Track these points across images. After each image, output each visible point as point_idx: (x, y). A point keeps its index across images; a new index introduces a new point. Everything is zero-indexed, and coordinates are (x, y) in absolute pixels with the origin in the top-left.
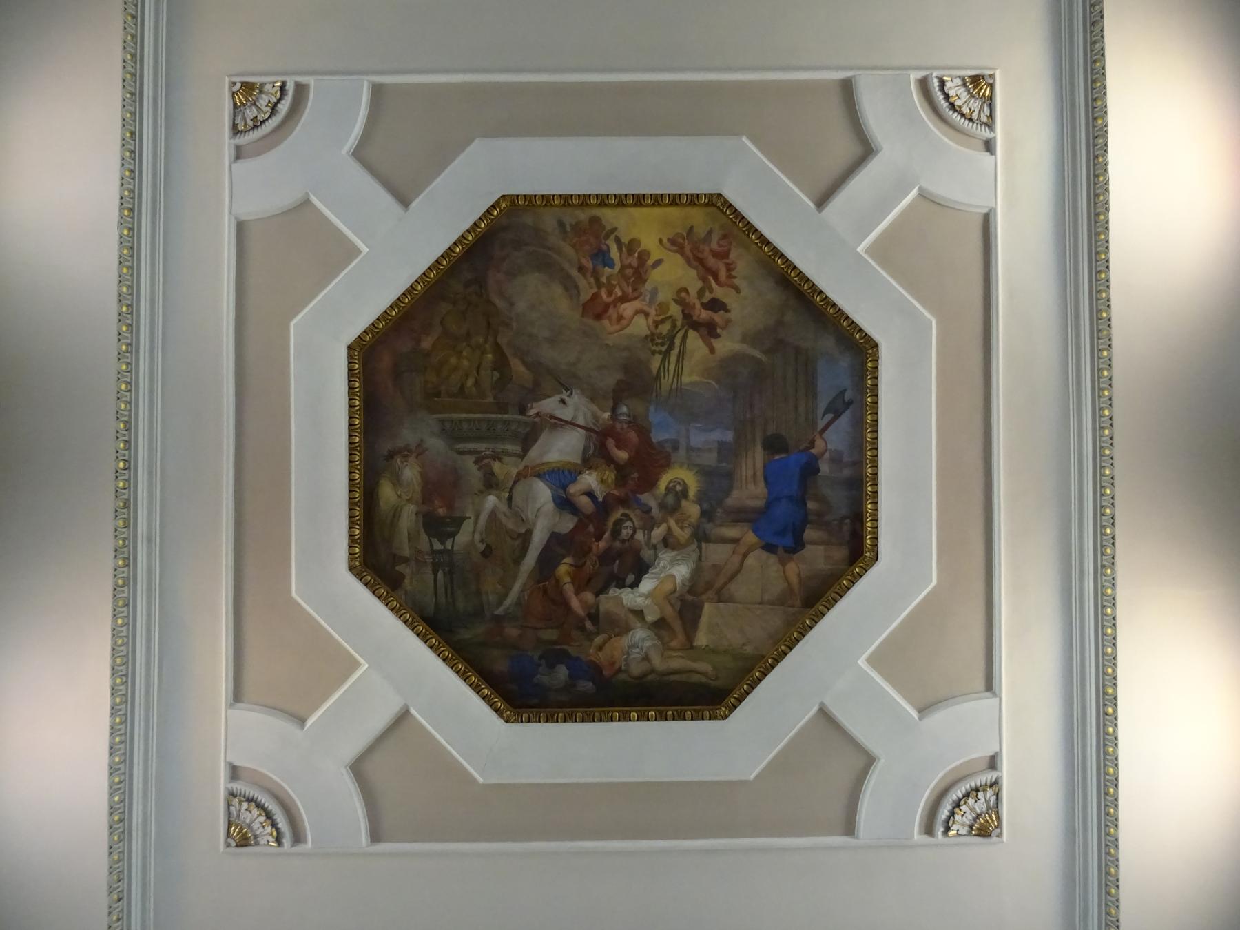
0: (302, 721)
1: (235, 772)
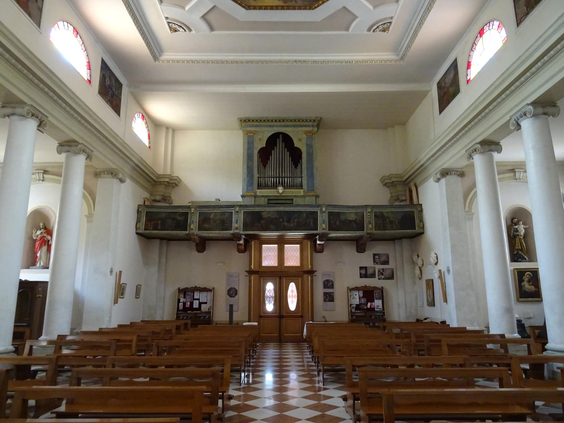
0: (184, 8)
1: (167, 18)
